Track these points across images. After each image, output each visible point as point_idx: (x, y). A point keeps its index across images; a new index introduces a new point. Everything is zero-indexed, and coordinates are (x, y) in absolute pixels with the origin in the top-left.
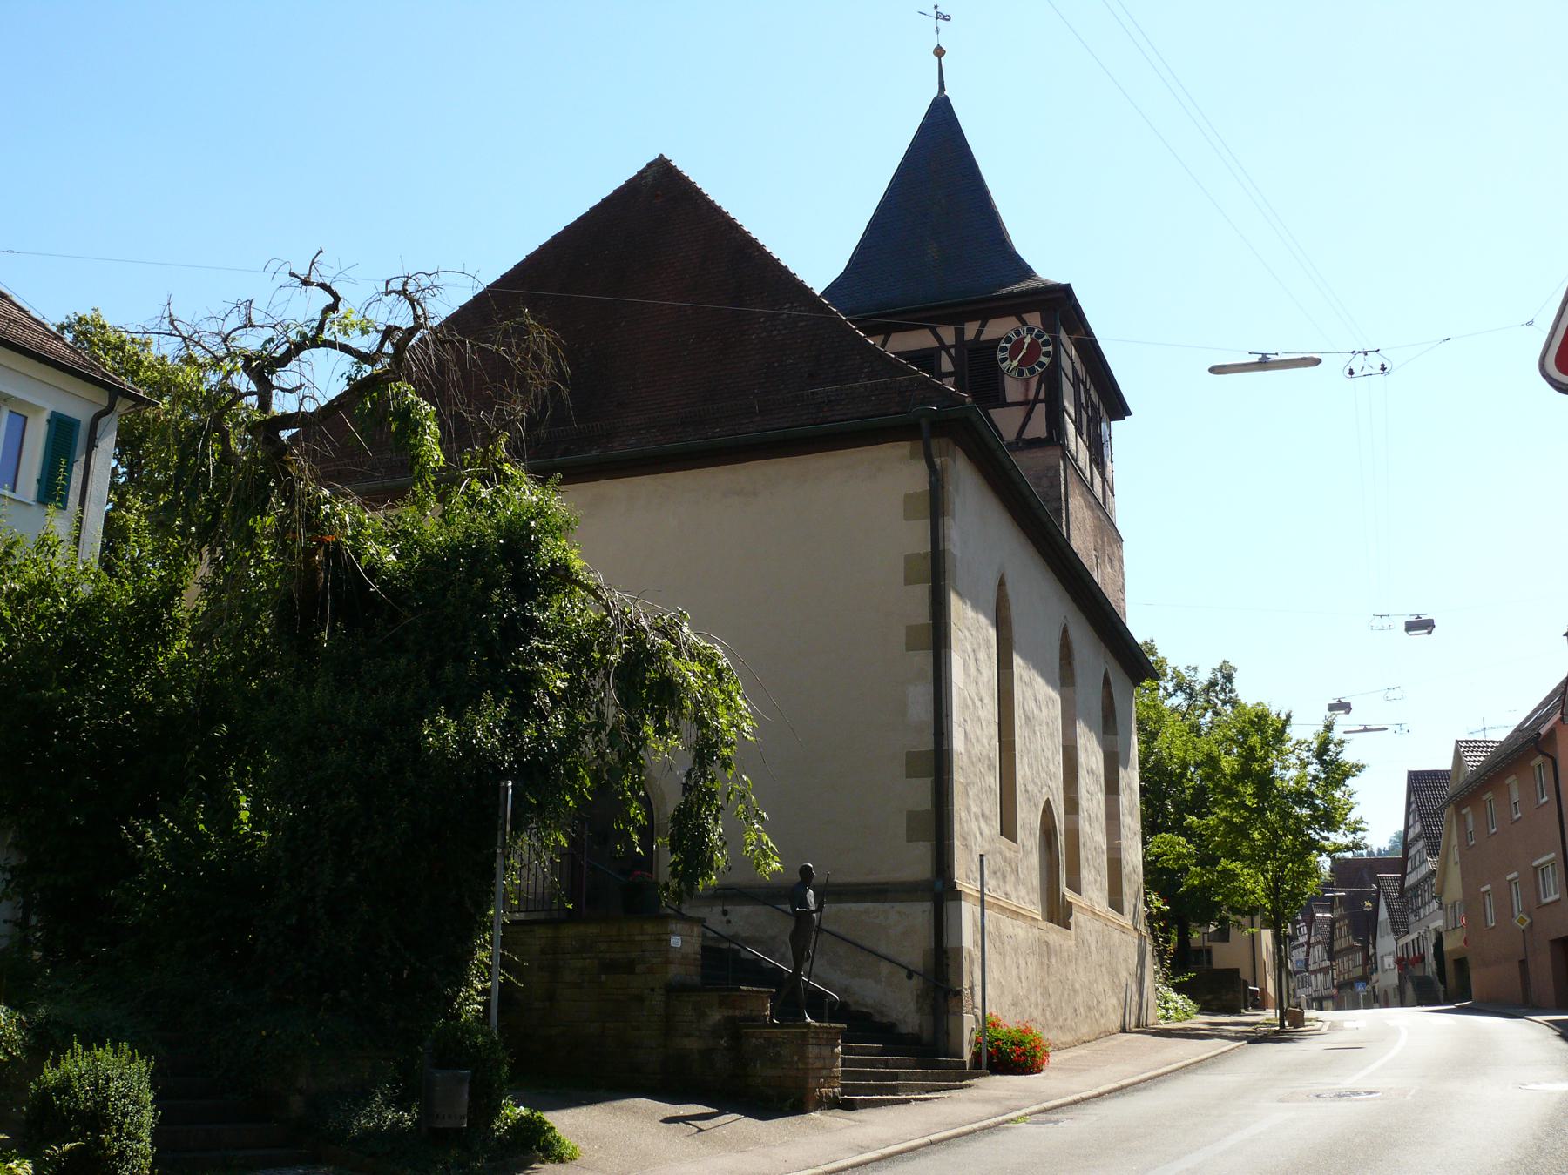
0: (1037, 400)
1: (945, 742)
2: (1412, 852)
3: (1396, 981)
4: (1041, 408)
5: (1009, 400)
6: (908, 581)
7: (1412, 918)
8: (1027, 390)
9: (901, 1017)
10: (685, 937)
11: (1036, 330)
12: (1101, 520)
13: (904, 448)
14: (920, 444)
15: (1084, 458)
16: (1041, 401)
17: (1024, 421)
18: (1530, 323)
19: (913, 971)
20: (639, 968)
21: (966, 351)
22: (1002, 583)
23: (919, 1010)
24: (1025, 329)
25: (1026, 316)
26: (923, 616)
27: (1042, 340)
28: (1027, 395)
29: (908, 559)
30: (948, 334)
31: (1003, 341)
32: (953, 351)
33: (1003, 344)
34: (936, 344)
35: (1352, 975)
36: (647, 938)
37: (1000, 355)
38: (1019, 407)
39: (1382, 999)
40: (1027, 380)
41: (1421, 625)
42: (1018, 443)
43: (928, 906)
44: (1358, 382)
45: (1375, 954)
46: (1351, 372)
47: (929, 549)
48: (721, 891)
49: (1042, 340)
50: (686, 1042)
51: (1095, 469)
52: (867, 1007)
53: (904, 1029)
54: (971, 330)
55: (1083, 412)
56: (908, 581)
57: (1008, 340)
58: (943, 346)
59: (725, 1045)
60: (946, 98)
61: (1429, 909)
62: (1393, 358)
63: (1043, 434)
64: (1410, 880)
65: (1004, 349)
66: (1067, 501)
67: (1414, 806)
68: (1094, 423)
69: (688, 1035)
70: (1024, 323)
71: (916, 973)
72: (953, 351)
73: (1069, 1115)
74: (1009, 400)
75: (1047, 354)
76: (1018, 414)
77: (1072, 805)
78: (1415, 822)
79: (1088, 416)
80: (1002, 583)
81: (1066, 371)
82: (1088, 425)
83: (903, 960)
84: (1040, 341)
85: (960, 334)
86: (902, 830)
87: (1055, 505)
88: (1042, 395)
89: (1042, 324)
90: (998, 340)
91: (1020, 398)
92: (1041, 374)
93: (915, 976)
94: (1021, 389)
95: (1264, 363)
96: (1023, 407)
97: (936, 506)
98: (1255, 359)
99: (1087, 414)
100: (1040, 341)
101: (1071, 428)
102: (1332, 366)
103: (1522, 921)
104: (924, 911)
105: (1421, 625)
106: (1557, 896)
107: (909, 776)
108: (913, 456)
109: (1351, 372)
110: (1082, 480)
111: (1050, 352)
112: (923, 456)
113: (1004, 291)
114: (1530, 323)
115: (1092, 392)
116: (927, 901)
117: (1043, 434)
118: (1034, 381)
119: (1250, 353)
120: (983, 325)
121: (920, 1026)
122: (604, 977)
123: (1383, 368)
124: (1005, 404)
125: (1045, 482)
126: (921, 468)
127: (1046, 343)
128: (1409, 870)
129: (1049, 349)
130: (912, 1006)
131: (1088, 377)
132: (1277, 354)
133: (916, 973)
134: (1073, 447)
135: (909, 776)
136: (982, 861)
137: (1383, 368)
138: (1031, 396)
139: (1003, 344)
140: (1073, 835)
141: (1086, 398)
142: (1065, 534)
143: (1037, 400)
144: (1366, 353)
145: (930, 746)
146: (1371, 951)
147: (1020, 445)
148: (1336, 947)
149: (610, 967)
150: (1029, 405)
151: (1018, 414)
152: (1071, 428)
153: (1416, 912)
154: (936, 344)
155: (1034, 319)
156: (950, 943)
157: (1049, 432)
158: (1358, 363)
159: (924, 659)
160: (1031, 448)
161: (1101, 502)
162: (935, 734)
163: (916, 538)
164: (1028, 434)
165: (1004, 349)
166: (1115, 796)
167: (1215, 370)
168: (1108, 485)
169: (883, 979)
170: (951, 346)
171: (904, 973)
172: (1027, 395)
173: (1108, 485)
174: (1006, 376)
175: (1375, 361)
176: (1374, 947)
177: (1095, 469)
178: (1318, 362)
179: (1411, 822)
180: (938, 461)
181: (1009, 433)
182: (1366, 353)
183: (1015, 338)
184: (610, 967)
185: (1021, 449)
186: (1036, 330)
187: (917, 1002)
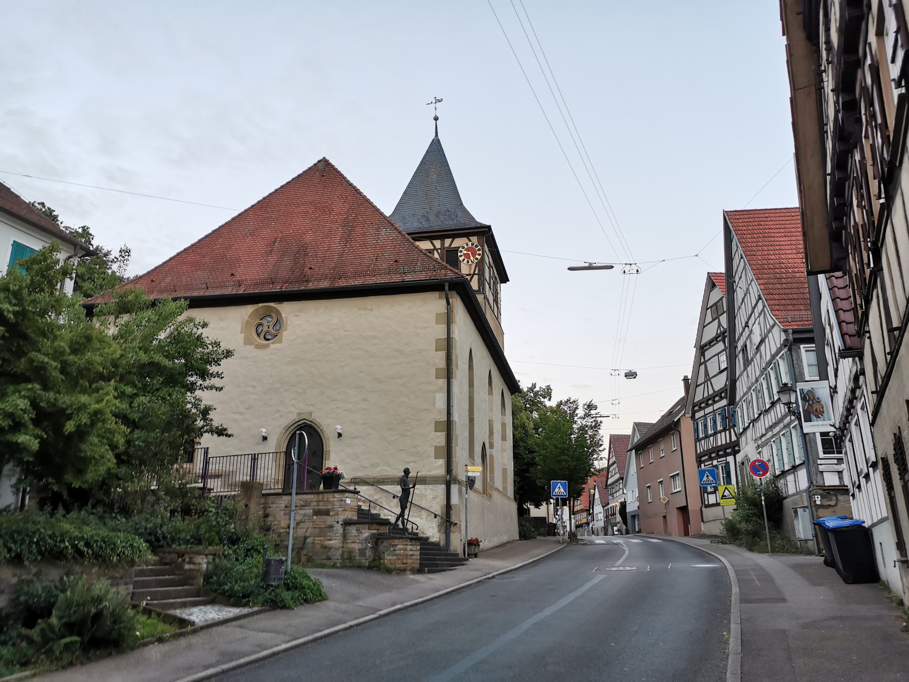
0: (474, 274)
1: (451, 417)
2: (611, 469)
3: (603, 525)
7: (610, 497)
9: (431, 534)
13: (436, 294)
14: (443, 294)
16: (476, 274)
18: (697, 256)
20: (331, 514)
22: (471, 350)
23: (439, 531)
24: (470, 243)
26: (442, 364)
30: (438, 243)
32: (439, 251)
33: (461, 249)
35: (582, 522)
36: (336, 499)
37: (459, 254)
39: (596, 532)
41: (631, 375)
43: (444, 486)
44: (627, 276)
45: (593, 512)
46: (624, 272)
50: (353, 545)
53: (432, 540)
54: (447, 242)
58: (435, 249)
61: (618, 494)
62: (642, 268)
64: (610, 482)
67: (612, 449)
68: (495, 284)
70: (470, 241)
72: (439, 251)
73: (512, 576)
75: (479, 255)
77: (491, 446)
78: (613, 456)
80: (471, 350)
83: (432, 510)
85: (443, 244)
86: (433, 454)
88: (477, 272)
90: (459, 247)
93: (438, 517)
94: (468, 268)
95: (590, 267)
97: (449, 320)
98: (587, 265)
101: (487, 286)
102: (617, 269)
103: (664, 499)
105: (631, 375)
106: (680, 489)
108: (440, 298)
109: (624, 272)
110: (491, 308)
113: (860, 317)
114: (697, 256)
115: (495, 271)
118: (474, 265)
120: (452, 242)
122: (315, 517)
123: (638, 271)
126: (444, 302)
127: (479, 250)
128: (609, 477)
129: (481, 252)
130: (436, 530)
137: (638, 271)
138: (472, 272)
143: (474, 274)
144: (631, 265)
145: (446, 419)
146: (591, 511)
148: (576, 509)
149: (317, 513)
152: (487, 286)
153: (612, 495)
155: (474, 239)
157: (479, 288)
158: (627, 268)
159: (442, 382)
162: (447, 414)
163: (440, 331)
167: (570, 269)
175: (634, 268)
176: (593, 510)
178: (612, 267)
179: (611, 456)
180: (450, 300)
182: (631, 265)
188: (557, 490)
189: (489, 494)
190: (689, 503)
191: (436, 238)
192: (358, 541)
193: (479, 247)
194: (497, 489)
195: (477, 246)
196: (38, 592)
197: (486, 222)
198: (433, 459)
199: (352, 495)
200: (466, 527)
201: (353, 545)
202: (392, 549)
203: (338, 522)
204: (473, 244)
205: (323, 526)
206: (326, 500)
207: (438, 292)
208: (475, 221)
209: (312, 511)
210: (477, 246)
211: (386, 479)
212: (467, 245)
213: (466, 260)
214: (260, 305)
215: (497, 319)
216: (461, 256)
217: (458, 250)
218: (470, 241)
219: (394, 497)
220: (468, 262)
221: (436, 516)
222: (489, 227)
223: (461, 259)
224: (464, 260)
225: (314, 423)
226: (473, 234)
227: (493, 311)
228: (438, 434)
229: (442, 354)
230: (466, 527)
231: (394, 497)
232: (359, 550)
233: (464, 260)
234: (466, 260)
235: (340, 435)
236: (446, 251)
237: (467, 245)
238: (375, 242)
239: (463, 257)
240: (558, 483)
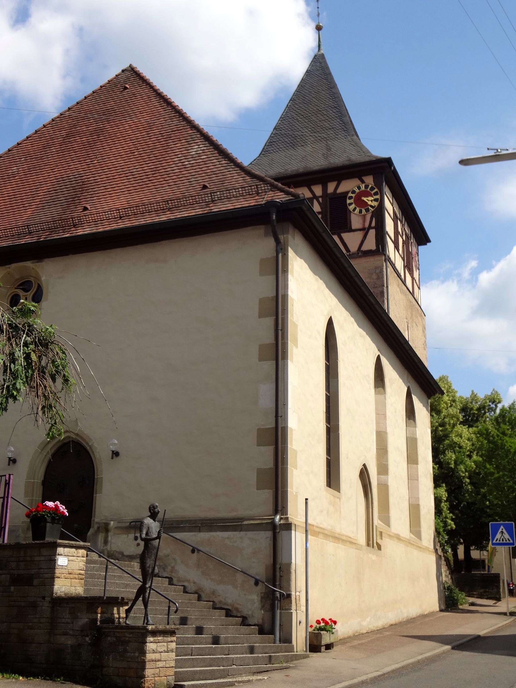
0: (370, 227)
4: (372, 233)
5: (353, 227)
6: (261, 316)
8: (364, 221)
9: (250, 613)
10: (71, 558)
11: (370, 186)
12: (411, 302)
13: (260, 230)
15: (399, 264)
16: (373, 228)
17: (362, 240)
19: (259, 580)
20: (36, 582)
21: (328, 199)
23: (263, 607)
24: (364, 185)
25: (364, 178)
26: (270, 339)
27: (369, 188)
28: (364, 225)
29: (262, 301)
30: (318, 190)
31: (350, 193)
32: (320, 199)
33: (350, 195)
34: (311, 196)
36: (43, 558)
37: (348, 201)
38: (359, 232)
40: (364, 216)
42: (358, 253)
43: (269, 534)
47: (275, 295)
48: (134, 523)
49: (369, 188)
51: (407, 272)
52: (228, 605)
54: (331, 187)
55: (400, 237)
56: (261, 316)
57: (354, 192)
58: (315, 197)
59: (89, 642)
60: (323, 55)
63: (373, 247)
65: (351, 198)
66: (387, 287)
69: (65, 634)
70: (363, 182)
71: (261, 581)
72: (320, 199)
74: (353, 227)
76: (359, 235)
77: (383, 469)
79: (403, 240)
81: (389, 211)
82: (403, 246)
83: (252, 572)
84: (368, 189)
85: (325, 189)
87: (380, 289)
88: (373, 224)
89: (374, 182)
90: (347, 193)
91: (360, 226)
92: (373, 212)
93: (260, 583)
94: (361, 221)
96: (362, 232)
98: (492, 153)
99: (403, 239)
100: (368, 189)
104: (267, 538)
107: (258, 445)
108: (266, 235)
110: (399, 276)
111: (378, 199)
112: (272, 234)
116: (268, 531)
117: (373, 247)
119: (488, 149)
121: (263, 619)
122: (12, 588)
124: (351, 230)
125: (374, 276)
130: (257, 604)
131: (403, 217)
132: (507, 150)
133: (261, 581)
134: (392, 256)
135: (258, 445)
136: (306, 503)
138: (367, 225)
139: (350, 195)
140: (384, 488)
141: (402, 229)
142: (387, 312)
143: (370, 227)
147: (360, 254)
149: (17, 580)
150: (365, 231)
151: (359, 235)
154: (311, 196)
155: (369, 180)
156: (282, 559)
159: (269, 366)
160: (365, 256)
161: (411, 291)
164: (364, 248)
165: (351, 198)
166: (415, 465)
168: (416, 282)
169: (239, 585)
170: (320, 197)
171: (253, 581)
172: (364, 225)
173: (416, 282)
174: (352, 214)
177: (407, 272)
181: (353, 248)
183: (357, 191)
184: (17, 580)
185: (360, 257)
186: (370, 186)
187: (261, 601)
188: (498, 536)
189: (377, 544)
190: (192, 545)
191: (316, 182)
192: (71, 632)
193: (376, 190)
194: (398, 538)
195: (372, 189)
196: (461, 604)
197: (384, 155)
198: (255, 490)
199: (73, 550)
200: (307, 600)
201: (62, 639)
202: (121, 648)
203: (44, 598)
204: (366, 187)
205: (23, 604)
206: (28, 559)
207: (262, 227)
208: (371, 155)
209: (8, 576)
210: (372, 189)
211: (182, 522)
212: (359, 188)
213: (358, 209)
214: (13, 266)
215: (412, 294)
216: (350, 204)
217: (346, 197)
218: (363, 182)
219: (193, 551)
220: (361, 211)
221: (257, 583)
222: (388, 161)
223: (351, 208)
224: (354, 209)
225: (81, 437)
226: (367, 173)
227: (404, 282)
228: (263, 449)
229: (269, 321)
230: (307, 600)
231: (193, 551)
232: (72, 646)
233: (354, 209)
234: (358, 209)
235: (115, 454)
236: (330, 199)
237: (359, 188)
238: (180, 164)
239: (353, 206)
240: (500, 525)
